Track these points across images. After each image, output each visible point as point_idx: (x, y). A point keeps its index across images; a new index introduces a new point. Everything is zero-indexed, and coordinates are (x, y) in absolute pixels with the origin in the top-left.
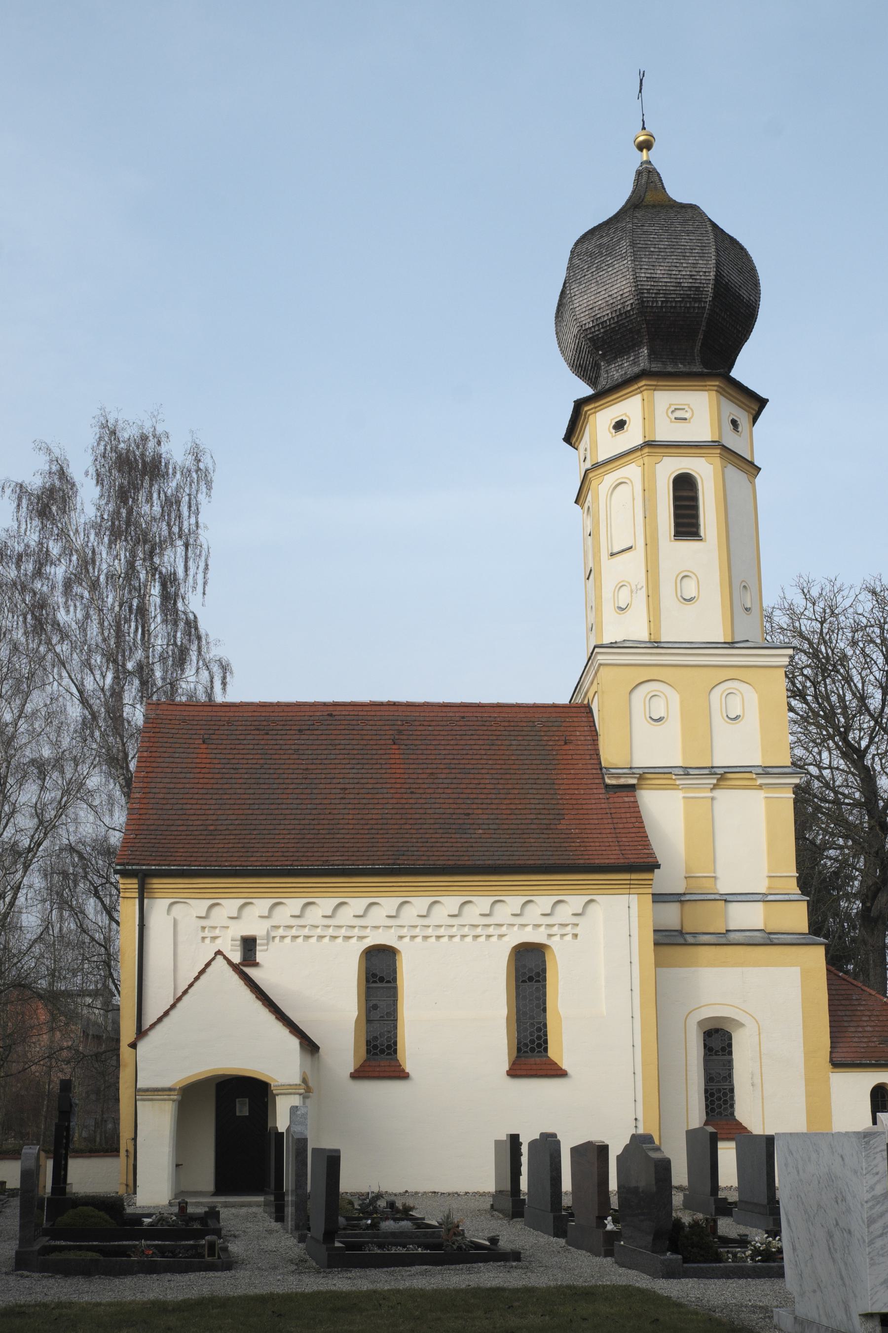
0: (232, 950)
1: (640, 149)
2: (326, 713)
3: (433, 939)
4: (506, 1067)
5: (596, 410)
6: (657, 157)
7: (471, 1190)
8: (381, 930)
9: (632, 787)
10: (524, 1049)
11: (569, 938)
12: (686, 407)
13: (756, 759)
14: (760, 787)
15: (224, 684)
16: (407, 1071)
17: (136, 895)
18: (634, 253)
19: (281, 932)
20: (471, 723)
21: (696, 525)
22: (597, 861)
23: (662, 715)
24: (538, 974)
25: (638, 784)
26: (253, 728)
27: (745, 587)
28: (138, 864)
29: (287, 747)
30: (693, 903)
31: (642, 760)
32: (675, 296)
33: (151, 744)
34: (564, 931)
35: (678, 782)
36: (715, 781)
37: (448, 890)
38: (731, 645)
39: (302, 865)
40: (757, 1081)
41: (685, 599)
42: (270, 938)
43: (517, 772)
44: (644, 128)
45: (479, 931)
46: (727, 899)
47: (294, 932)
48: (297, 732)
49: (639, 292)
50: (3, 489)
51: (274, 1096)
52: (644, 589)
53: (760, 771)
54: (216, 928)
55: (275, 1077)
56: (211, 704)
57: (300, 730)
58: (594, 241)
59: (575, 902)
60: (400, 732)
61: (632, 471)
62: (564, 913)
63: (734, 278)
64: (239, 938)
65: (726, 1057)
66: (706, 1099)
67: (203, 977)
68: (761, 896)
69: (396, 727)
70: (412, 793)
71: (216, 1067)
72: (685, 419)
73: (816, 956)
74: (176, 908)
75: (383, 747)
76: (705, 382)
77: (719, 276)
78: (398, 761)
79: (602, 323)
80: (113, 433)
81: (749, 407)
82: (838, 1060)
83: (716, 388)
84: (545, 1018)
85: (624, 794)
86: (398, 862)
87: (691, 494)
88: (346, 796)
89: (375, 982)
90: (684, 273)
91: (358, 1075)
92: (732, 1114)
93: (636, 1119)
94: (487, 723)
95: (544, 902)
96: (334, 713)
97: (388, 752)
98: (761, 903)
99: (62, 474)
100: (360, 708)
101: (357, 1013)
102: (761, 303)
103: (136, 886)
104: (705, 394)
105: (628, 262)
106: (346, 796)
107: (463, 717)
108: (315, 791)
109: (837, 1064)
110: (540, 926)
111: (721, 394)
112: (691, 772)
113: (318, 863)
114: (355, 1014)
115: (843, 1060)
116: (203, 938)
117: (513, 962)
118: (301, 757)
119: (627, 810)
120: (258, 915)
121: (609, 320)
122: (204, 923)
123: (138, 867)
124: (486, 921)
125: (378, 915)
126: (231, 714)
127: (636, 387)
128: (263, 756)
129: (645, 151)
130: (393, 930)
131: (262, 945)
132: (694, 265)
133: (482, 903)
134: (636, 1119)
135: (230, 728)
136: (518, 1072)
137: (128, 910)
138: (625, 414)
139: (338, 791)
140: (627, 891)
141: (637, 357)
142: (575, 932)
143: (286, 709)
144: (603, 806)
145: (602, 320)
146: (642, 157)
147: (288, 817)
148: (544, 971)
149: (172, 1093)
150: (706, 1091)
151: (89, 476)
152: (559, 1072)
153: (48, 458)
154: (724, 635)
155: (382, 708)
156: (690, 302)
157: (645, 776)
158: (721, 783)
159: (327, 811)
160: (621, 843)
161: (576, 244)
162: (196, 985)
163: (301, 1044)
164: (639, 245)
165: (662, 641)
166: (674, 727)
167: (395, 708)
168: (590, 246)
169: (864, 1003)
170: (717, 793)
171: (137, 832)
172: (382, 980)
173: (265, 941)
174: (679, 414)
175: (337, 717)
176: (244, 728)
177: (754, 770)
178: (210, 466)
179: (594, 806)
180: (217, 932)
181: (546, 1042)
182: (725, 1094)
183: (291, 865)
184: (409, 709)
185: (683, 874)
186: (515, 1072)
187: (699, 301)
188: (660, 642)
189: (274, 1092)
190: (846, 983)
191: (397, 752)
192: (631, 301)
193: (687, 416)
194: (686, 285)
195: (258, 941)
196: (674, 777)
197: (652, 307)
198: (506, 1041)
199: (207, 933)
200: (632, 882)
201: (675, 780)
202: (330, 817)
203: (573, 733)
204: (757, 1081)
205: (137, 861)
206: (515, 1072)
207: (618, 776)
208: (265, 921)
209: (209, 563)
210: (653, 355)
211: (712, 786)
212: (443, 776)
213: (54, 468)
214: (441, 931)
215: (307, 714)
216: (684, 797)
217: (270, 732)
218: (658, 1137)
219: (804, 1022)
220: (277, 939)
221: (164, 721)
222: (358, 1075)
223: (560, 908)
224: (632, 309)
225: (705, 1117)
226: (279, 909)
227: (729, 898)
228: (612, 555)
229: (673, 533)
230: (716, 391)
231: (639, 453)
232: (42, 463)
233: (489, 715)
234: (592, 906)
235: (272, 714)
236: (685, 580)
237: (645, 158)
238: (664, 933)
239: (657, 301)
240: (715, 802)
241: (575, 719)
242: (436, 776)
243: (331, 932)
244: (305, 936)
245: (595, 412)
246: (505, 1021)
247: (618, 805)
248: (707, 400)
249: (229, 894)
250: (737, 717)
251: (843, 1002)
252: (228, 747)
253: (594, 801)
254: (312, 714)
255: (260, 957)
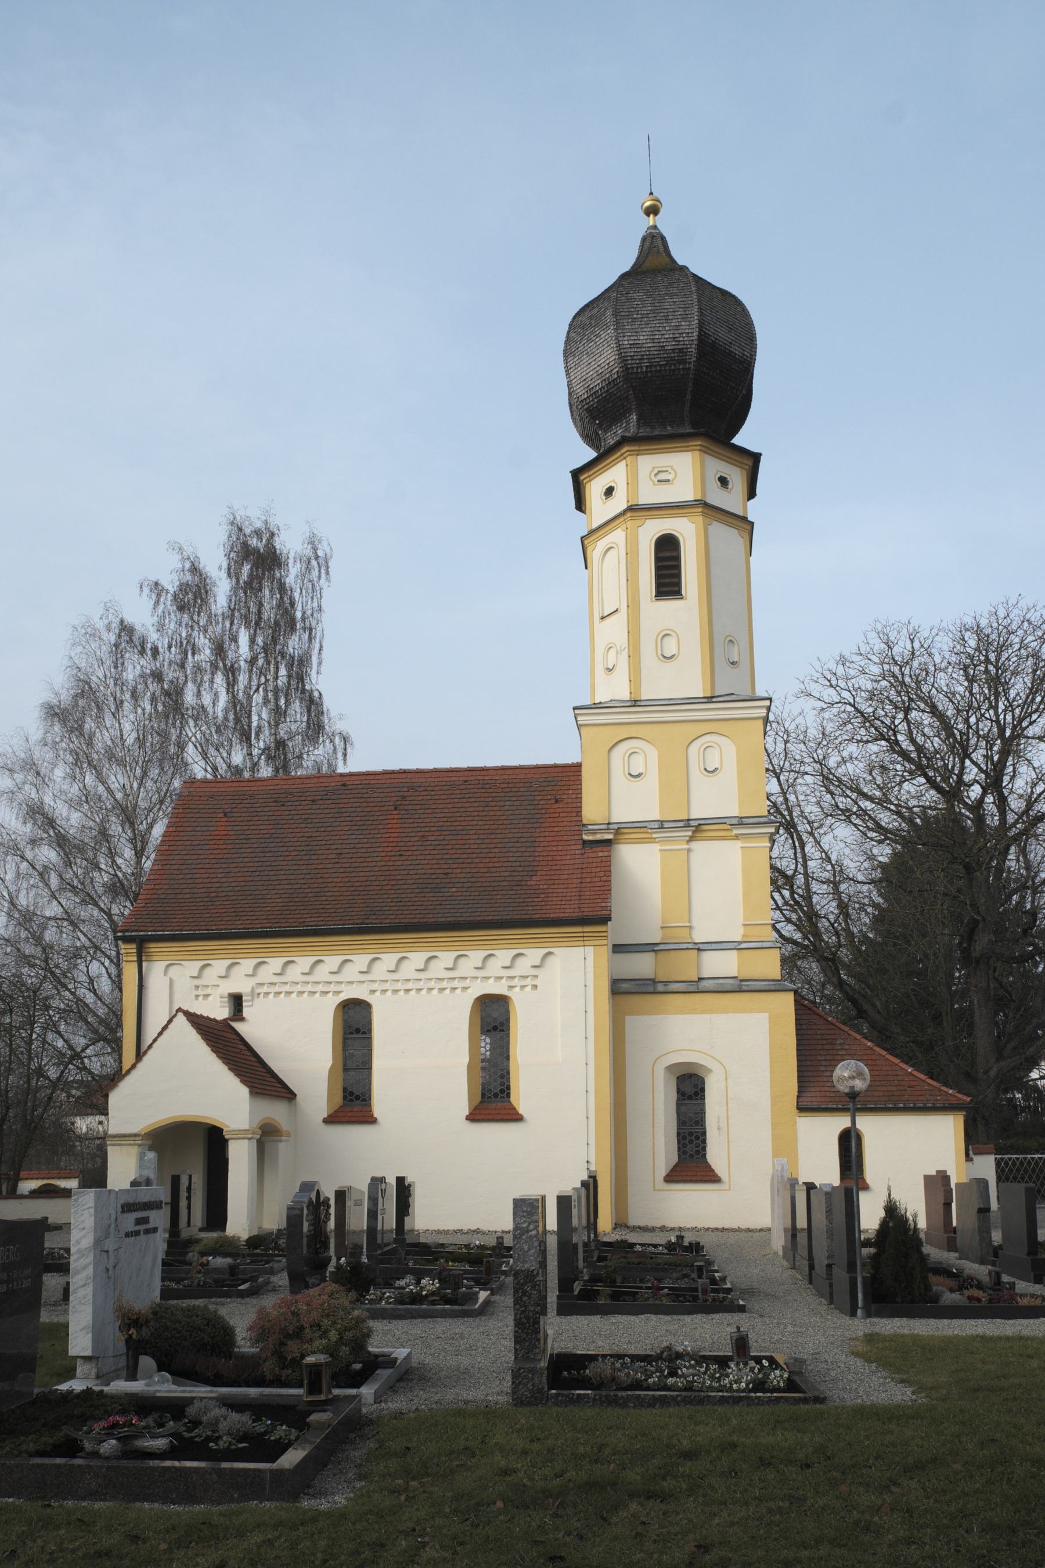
0: (221, 1007)
1: (648, 215)
2: (339, 784)
3: (402, 993)
4: (466, 1112)
5: (591, 478)
6: (664, 223)
7: (431, 1228)
8: (354, 985)
9: (608, 842)
10: (349, 1098)
11: (528, 989)
12: (669, 469)
13: (732, 809)
14: (737, 837)
15: (345, 755)
16: (375, 1116)
17: (135, 959)
18: (617, 322)
19: (265, 989)
20: (472, 786)
21: (678, 584)
22: (552, 915)
23: (641, 771)
24: (502, 1024)
25: (614, 839)
26: (272, 800)
27: (731, 641)
28: (136, 931)
29: (298, 817)
30: (666, 952)
31: (620, 815)
32: (659, 360)
33: (178, 820)
34: (523, 983)
35: (654, 836)
36: (690, 833)
37: (413, 947)
38: (710, 699)
39: (279, 927)
40: (724, 1125)
41: (665, 657)
42: (254, 994)
43: (504, 831)
44: (651, 194)
45: (445, 984)
46: (700, 948)
47: (277, 989)
48: (310, 803)
49: (623, 359)
50: (141, 587)
51: (227, 1141)
52: (626, 650)
53: (735, 821)
54: (208, 986)
55: (227, 1123)
56: (333, 776)
57: (313, 801)
58: (588, 314)
59: (534, 955)
60: (404, 798)
61: (617, 536)
62: (524, 966)
63: (722, 334)
64: (227, 995)
65: (700, 1101)
66: (679, 1142)
67: (166, 1033)
68: (736, 944)
69: (401, 794)
70: (401, 855)
71: (178, 1114)
72: (669, 481)
73: (787, 1001)
74: (172, 969)
75: (385, 813)
76: (688, 442)
77: (703, 336)
78: (395, 826)
79: (595, 393)
80: (240, 529)
81: (741, 463)
82: (803, 1104)
83: (699, 448)
84: (508, 1066)
85: (600, 849)
86: (367, 921)
87: (674, 554)
88: (340, 861)
89: (351, 1033)
90: (667, 336)
91: (331, 1120)
92: (704, 1156)
93: (588, 1162)
94: (486, 786)
95: (504, 956)
96: (348, 783)
97: (388, 817)
98: (735, 952)
99: (195, 569)
100: (373, 777)
101: (331, 1063)
102: (757, 358)
103: (135, 951)
104: (689, 454)
105: (611, 331)
106: (340, 861)
107: (466, 781)
108: (313, 857)
109: (803, 1108)
110: (502, 978)
111: (706, 453)
112: (666, 825)
113: (294, 924)
114: (329, 1063)
115: (810, 1105)
116: (197, 996)
117: (341, 1013)
118: (309, 826)
119: (599, 865)
120: (414, 968)
121: (600, 389)
122: (197, 982)
123: (136, 934)
124: (451, 974)
125: (351, 972)
126: (255, 788)
127: (619, 454)
128: (275, 827)
129: (651, 216)
130: (365, 985)
131: (247, 1001)
132: (677, 328)
133: (446, 958)
134: (588, 1162)
135: (252, 801)
136: (477, 1117)
137: (130, 972)
138: (613, 481)
139: (334, 856)
140: (582, 943)
141: (628, 423)
142: (534, 983)
143: (565, 770)
144: (577, 861)
145: (594, 390)
146: (649, 222)
147: (283, 882)
148: (508, 1020)
149: (137, 1138)
150: (678, 1134)
151: (223, 571)
152: (369, 1119)
153: (180, 557)
154: (704, 690)
155: (393, 776)
156: (675, 364)
157: (620, 831)
158: (698, 835)
159: (319, 876)
160: (582, 898)
161: (574, 318)
162: (159, 1039)
163: (251, 1092)
164: (622, 314)
165: (642, 699)
166: (652, 780)
167: (404, 775)
168: (583, 318)
169: (847, 1047)
170: (694, 845)
171: (146, 901)
172: (358, 1031)
173: (250, 998)
174: (662, 476)
175: (349, 787)
176: (264, 800)
177: (728, 821)
178: (328, 551)
179: (567, 862)
180: (209, 991)
181: (509, 1088)
182: (697, 1138)
183: (380, 923)
184: (418, 775)
185: (660, 924)
186: (474, 1117)
187: (684, 362)
188: (640, 701)
189: (226, 1137)
190: (834, 1027)
191: (396, 817)
192: (617, 369)
193: (670, 477)
194: (669, 348)
195: (244, 998)
196: (650, 831)
197: (637, 373)
198: (466, 1087)
199: (200, 992)
200: (585, 935)
201: (651, 833)
202: (321, 880)
203: (566, 792)
204: (724, 1125)
205: (136, 928)
206: (474, 1117)
207: (594, 832)
208: (250, 978)
209: (324, 644)
210: (642, 421)
211: (688, 838)
212: (433, 838)
213: (188, 565)
214: (410, 985)
215: (323, 785)
216: (660, 850)
217: (286, 804)
218: (727, 1176)
219: (771, 1067)
220: (262, 996)
221: (195, 798)
222: (331, 1120)
223: (520, 961)
224: (618, 377)
225: (675, 1159)
226: (263, 967)
227: (701, 947)
228: (602, 618)
229: (654, 594)
230: (700, 450)
231: (622, 519)
232: (174, 562)
233: (490, 777)
234: (551, 959)
235: (292, 787)
236: (666, 638)
237: (651, 223)
238: (638, 982)
239: (641, 367)
240: (692, 854)
241: (572, 778)
242: (426, 838)
243: (309, 988)
244: (286, 992)
245: (590, 481)
246: (466, 1068)
247: (590, 860)
248: (690, 461)
249: (274, 953)
250: (639, 775)
251: (826, 1047)
252: (246, 819)
253: (568, 857)
254: (327, 784)
255: (246, 1012)
